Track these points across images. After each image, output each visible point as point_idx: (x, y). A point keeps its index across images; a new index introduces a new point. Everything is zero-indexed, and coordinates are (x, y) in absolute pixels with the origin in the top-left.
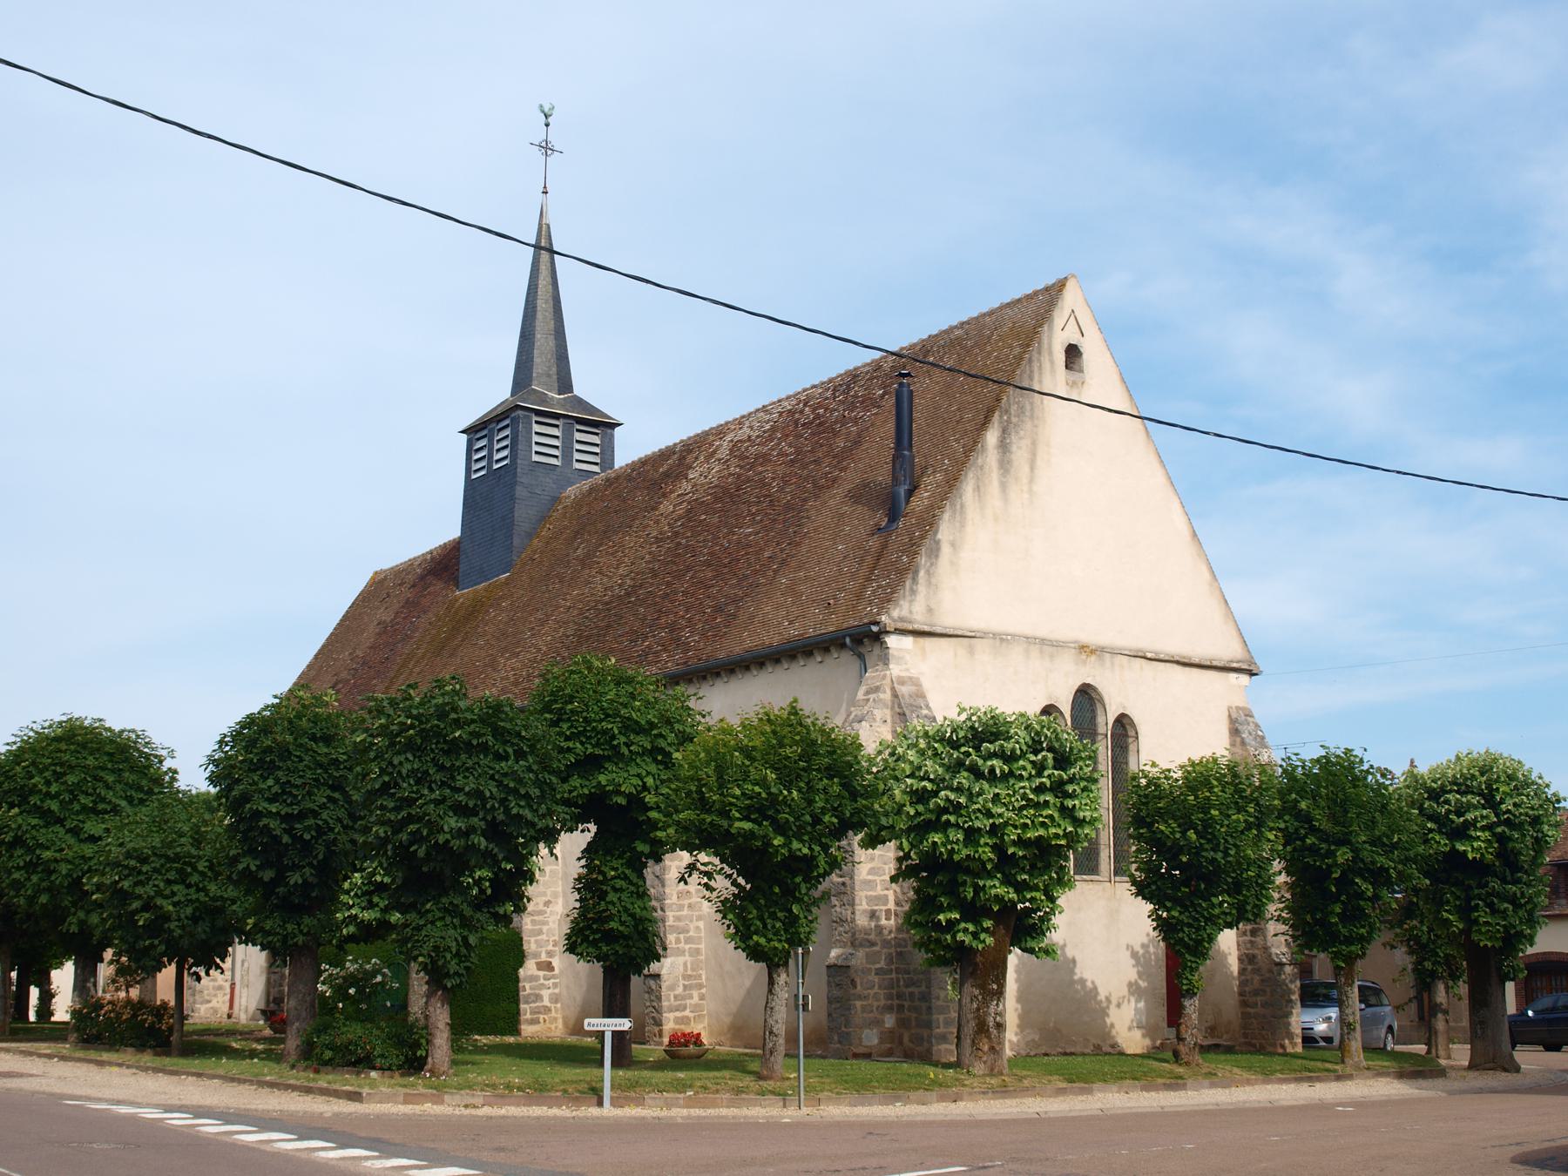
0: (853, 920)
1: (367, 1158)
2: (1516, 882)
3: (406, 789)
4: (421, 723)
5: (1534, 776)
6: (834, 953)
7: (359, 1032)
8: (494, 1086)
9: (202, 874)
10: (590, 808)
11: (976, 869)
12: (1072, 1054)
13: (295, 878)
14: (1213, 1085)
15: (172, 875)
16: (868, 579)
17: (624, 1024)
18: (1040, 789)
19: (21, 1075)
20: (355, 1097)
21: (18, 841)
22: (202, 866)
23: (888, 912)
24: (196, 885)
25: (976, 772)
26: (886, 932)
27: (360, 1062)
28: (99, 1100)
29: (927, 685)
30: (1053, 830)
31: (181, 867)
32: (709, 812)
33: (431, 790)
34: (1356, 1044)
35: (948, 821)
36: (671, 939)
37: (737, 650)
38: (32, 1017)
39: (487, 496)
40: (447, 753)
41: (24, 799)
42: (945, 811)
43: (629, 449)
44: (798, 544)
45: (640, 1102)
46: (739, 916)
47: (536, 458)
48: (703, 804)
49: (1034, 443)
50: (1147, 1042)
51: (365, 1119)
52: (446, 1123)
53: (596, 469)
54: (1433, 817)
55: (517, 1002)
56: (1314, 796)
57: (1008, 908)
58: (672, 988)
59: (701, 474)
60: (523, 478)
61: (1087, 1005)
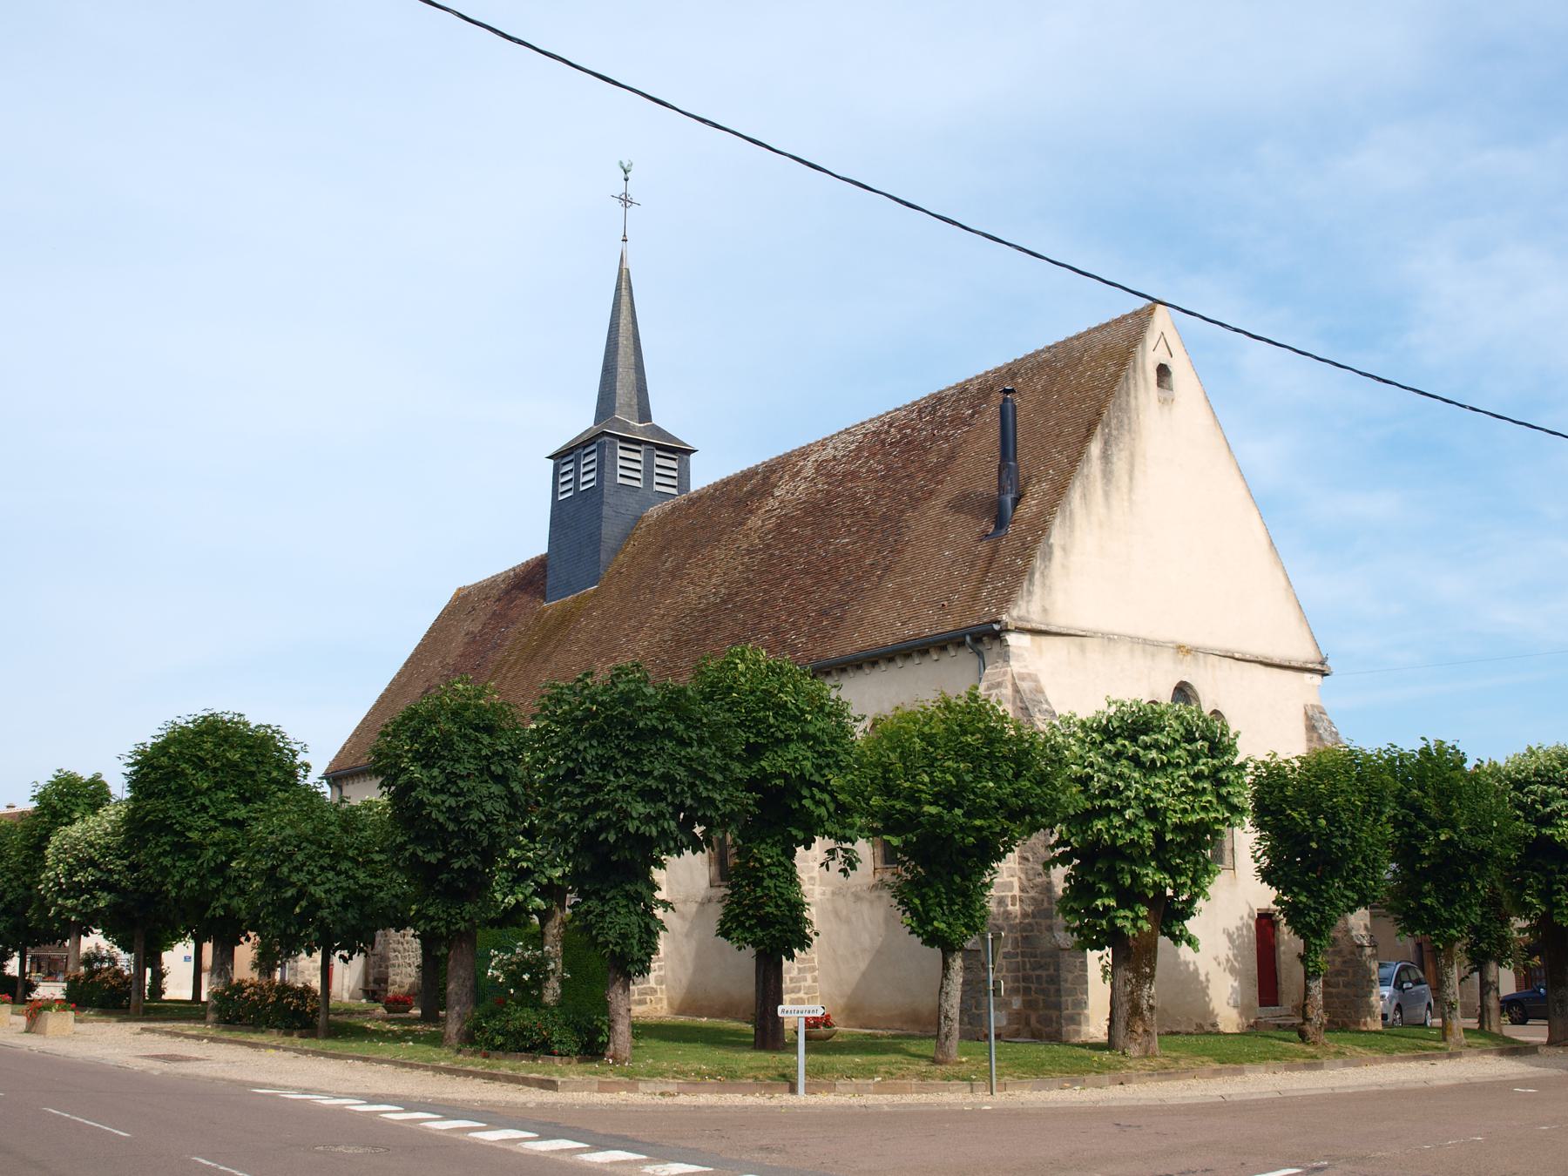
1: (580, 1150)
3: (590, 774)
7: (534, 1018)
12: (1178, 1033)
16: (982, 582)
20: (550, 1085)
23: (1013, 897)
24: (346, 872)
25: (1136, 761)
29: (1045, 681)
32: (897, 797)
33: (617, 775)
39: (574, 516)
43: (704, 474)
44: (901, 552)
45: (831, 1088)
47: (620, 480)
48: (888, 790)
49: (1132, 455)
51: (570, 1108)
53: (674, 491)
54: (1520, 806)
60: (609, 499)
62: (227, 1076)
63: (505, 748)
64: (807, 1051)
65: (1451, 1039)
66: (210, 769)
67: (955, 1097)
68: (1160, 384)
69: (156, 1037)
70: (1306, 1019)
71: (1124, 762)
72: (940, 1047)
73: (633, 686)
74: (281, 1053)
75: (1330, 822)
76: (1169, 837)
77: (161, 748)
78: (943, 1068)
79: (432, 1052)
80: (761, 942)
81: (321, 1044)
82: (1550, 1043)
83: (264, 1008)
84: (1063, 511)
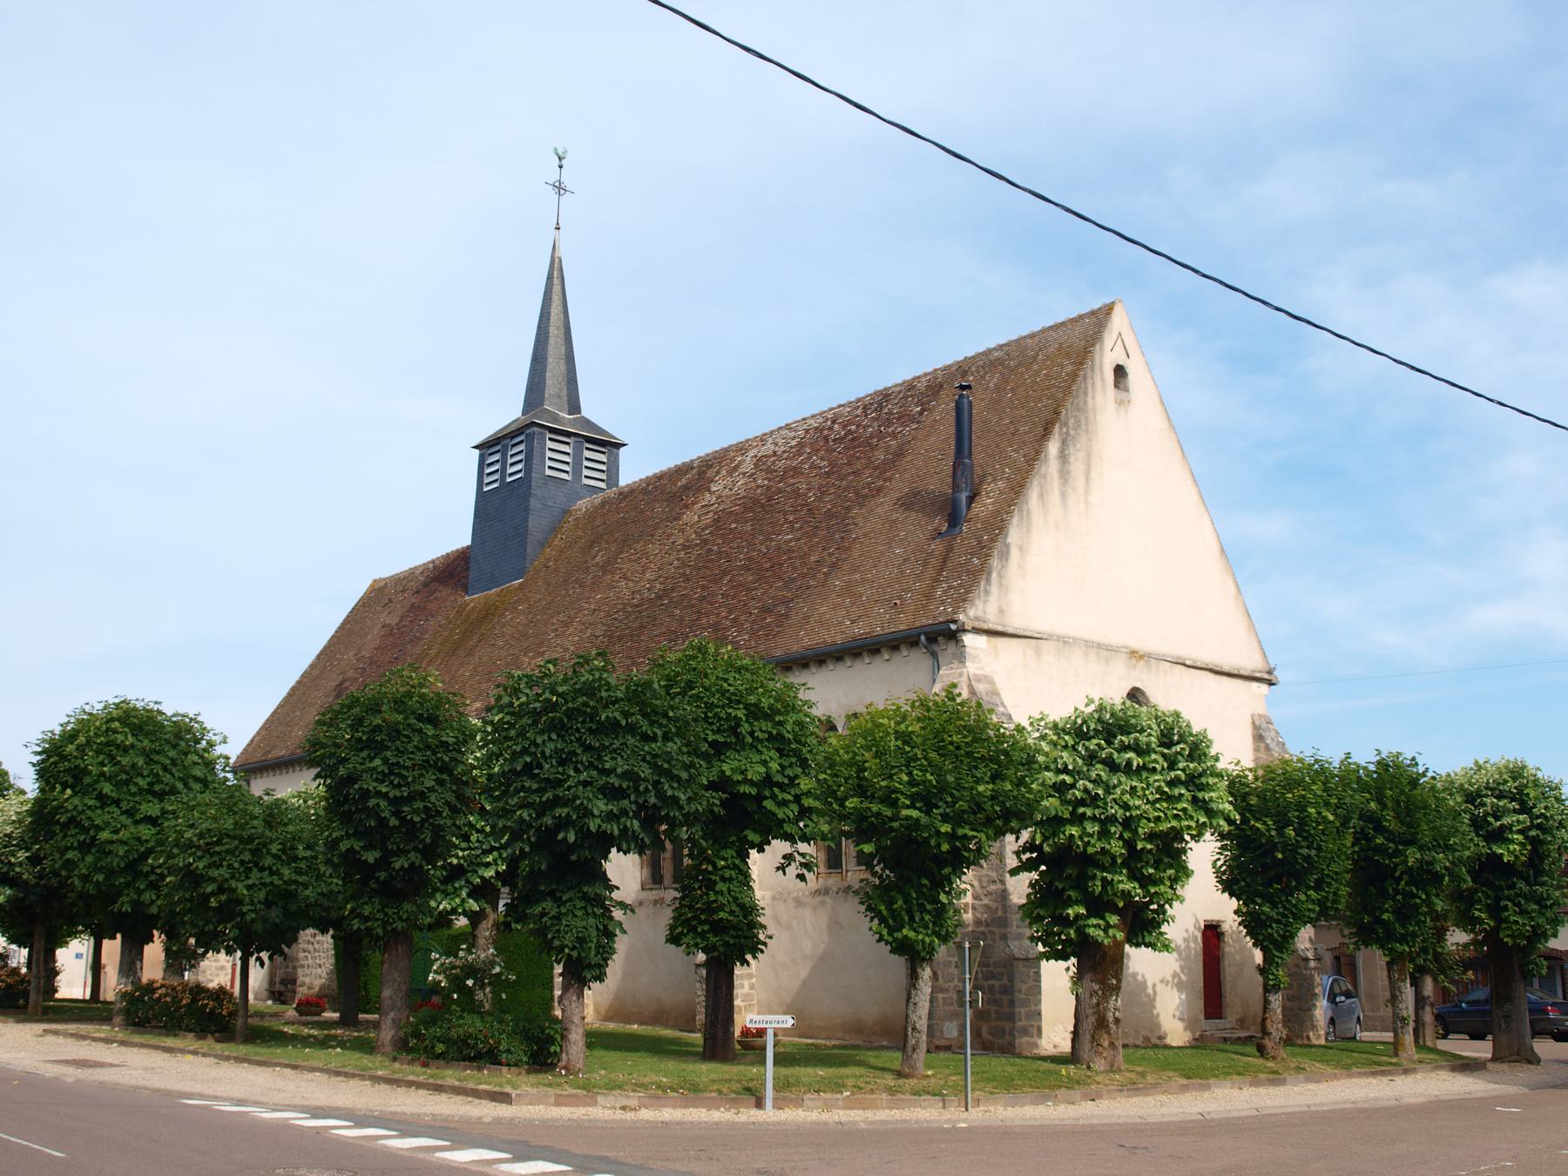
7: (479, 1024)
11: (1103, 861)
13: (399, 863)
16: (936, 580)
18: (1172, 783)
19: (102, 1065)
20: (503, 1098)
22: (275, 848)
24: (270, 868)
29: (1000, 684)
33: (577, 770)
35: (1084, 814)
37: (795, 648)
39: (499, 508)
42: (1082, 802)
43: (633, 469)
45: (799, 1103)
49: (1089, 456)
51: (529, 1124)
53: (603, 485)
60: (537, 491)
62: (149, 1084)
63: (451, 740)
65: (1403, 1055)
66: (118, 759)
67: (926, 1113)
68: (1117, 385)
69: (61, 1040)
70: (1265, 1032)
71: (1099, 766)
72: (907, 1059)
74: (200, 1058)
77: (70, 736)
78: (912, 1082)
79: (366, 1060)
80: (714, 947)
81: (243, 1050)
82: (1494, 1059)
83: (177, 1010)
84: (1021, 511)
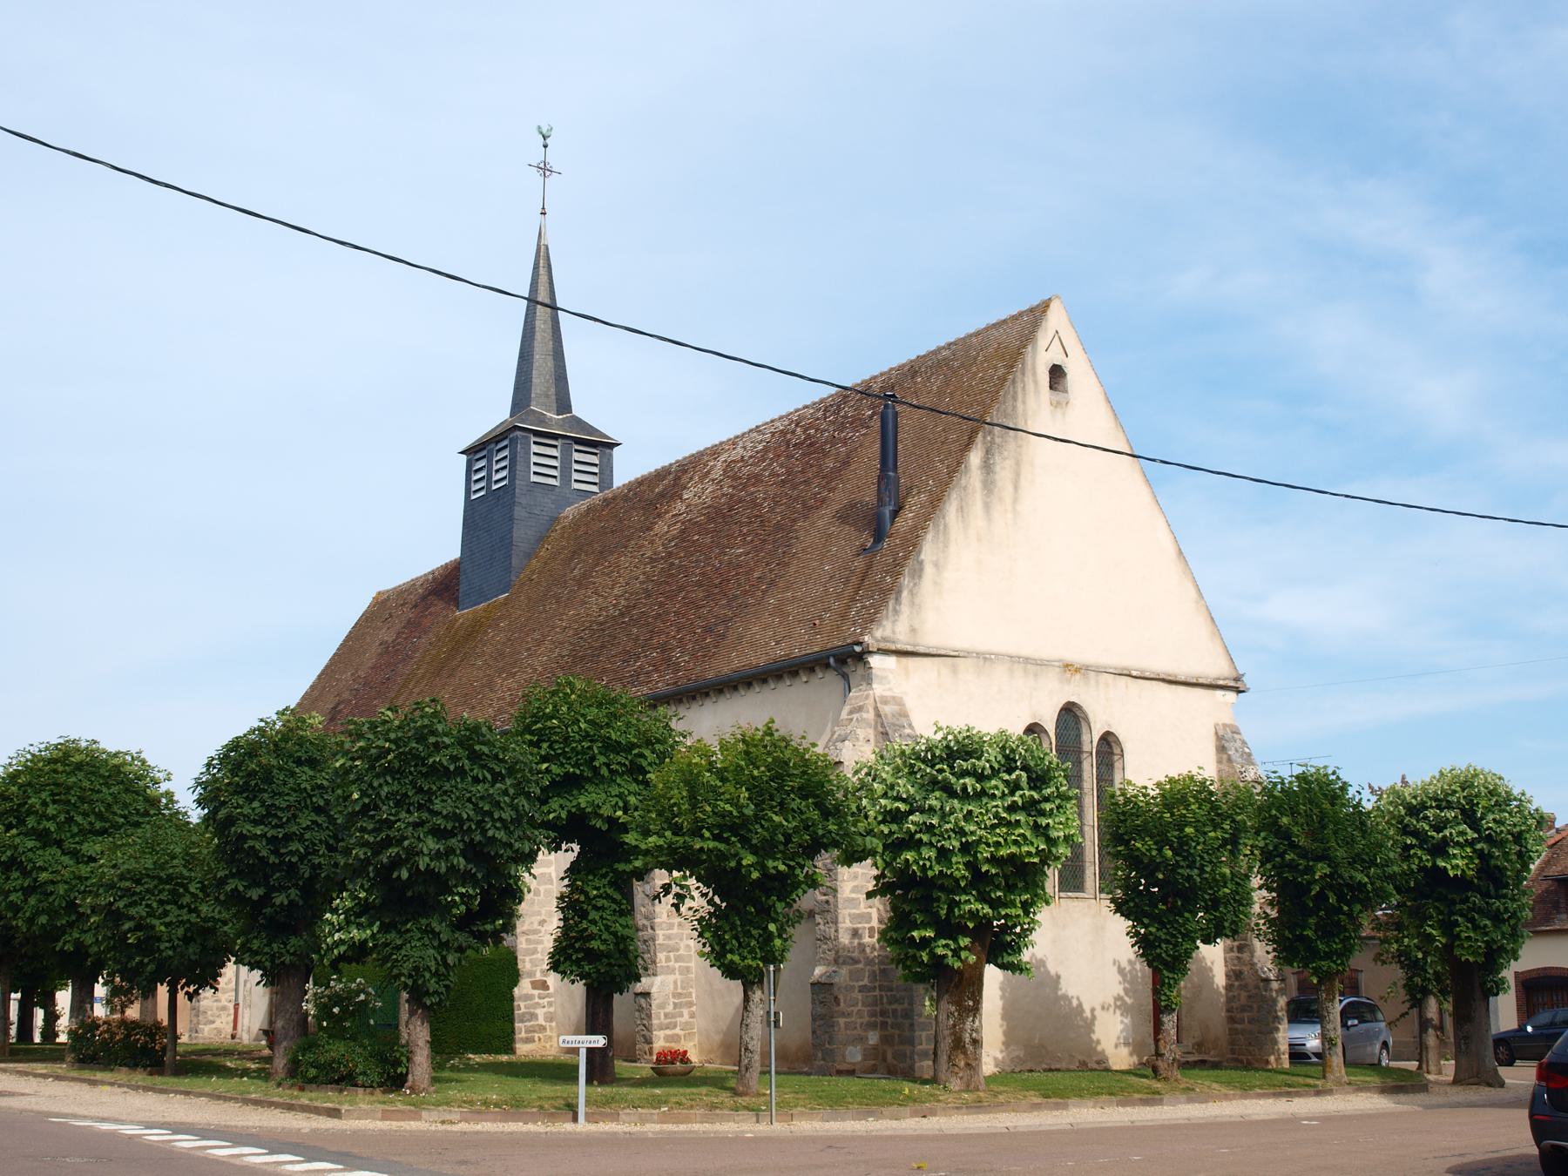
0: (836, 938)
2: (1498, 897)
4: (398, 747)
5: (1516, 792)
6: (818, 971)
8: (471, 1103)
9: (193, 895)
10: (560, 834)
12: (1058, 1070)
13: (280, 899)
14: (1190, 1101)
15: (164, 896)
16: (853, 600)
17: (599, 1041)
18: (1012, 808)
20: (334, 1113)
21: (12, 864)
23: (871, 929)
24: (188, 905)
26: (868, 950)
27: (344, 1079)
28: (85, 1117)
29: (910, 704)
30: (1025, 849)
31: (176, 887)
34: (1337, 1060)
35: (921, 840)
36: (661, 956)
37: (726, 670)
38: (37, 1039)
39: (486, 516)
40: (425, 776)
41: (21, 822)
43: (628, 468)
44: (787, 565)
45: (615, 1118)
46: (715, 935)
47: (534, 478)
49: (1018, 464)
50: (1135, 1059)
51: (342, 1135)
52: (418, 1139)
53: (594, 489)
55: (512, 1021)
56: (1293, 813)
57: (984, 925)
58: (662, 1006)
59: (696, 494)
60: (522, 498)
61: (1074, 1022)
64: (589, 1081)
73: (426, 721)
75: (1175, 853)
76: (984, 868)
82: (1456, 1082)
84: (936, 526)
